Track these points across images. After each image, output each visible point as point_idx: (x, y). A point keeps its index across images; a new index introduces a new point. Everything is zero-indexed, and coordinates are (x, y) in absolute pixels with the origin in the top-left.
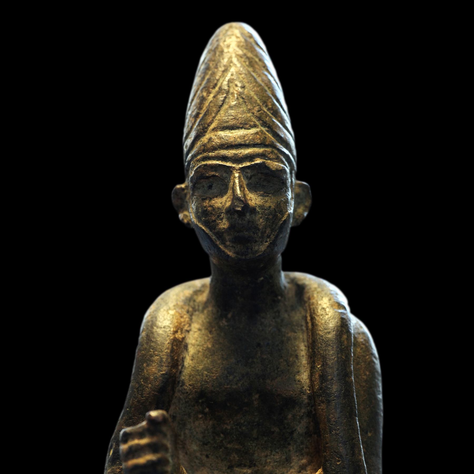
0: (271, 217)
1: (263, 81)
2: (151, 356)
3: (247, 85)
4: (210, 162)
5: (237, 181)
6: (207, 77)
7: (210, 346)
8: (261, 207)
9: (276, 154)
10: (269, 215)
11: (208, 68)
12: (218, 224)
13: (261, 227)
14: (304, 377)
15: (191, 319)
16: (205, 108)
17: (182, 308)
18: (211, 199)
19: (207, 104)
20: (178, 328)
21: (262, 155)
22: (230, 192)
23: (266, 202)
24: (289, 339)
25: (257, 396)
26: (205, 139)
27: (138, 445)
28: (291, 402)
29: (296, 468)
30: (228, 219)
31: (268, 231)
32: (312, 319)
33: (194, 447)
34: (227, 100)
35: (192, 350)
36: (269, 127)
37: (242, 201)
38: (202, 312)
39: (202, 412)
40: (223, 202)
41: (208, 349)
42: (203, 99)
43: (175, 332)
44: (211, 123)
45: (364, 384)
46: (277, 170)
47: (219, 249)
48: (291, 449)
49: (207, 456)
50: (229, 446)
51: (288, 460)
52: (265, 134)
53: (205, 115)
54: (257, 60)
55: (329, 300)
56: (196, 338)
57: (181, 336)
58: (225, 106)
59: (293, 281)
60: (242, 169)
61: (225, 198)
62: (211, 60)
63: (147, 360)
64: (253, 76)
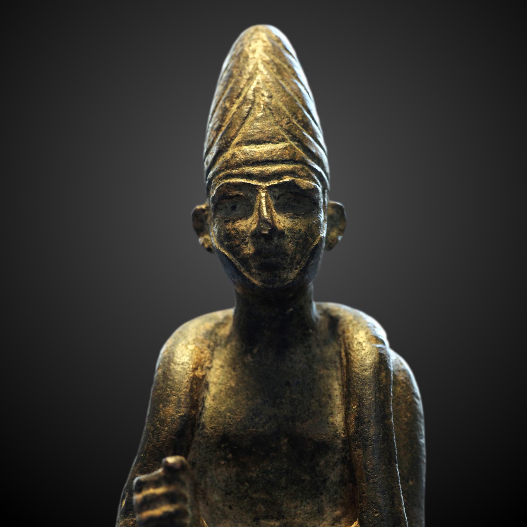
0: (301, 241)
1: (292, 90)
2: (168, 396)
3: (274, 94)
4: (233, 180)
5: (263, 201)
6: (230, 86)
7: (233, 385)
8: (290, 230)
9: (307, 171)
10: (299, 239)
11: (231, 76)
12: (242, 250)
13: (290, 253)
14: (338, 419)
15: (212, 355)
16: (227, 120)
17: (202, 342)
18: (234, 221)
19: (230, 115)
20: (198, 365)
21: (291, 173)
22: (255, 213)
23: (296, 224)
24: (321, 377)
25: (286, 441)
26: (227, 155)
27: (153, 495)
28: (323, 447)
29: (330, 520)
30: (253, 244)
31: (298, 257)
32: (347, 354)
33: (216, 497)
34: (252, 111)
35: (213, 390)
36: (299, 141)
37: (270, 224)
38: (225, 346)
39: (225, 458)
40: (247, 225)
41: (231, 388)
42: (225, 111)
43: (195, 369)
44: (235, 136)
45: (405, 427)
46: (308, 189)
47: (243, 277)
48: (324, 499)
49: (230, 507)
50: (254, 496)
51: (320, 512)
52: (295, 149)
53: (228, 128)
54: (286, 67)
55: (366, 334)
56: (217, 376)
57: (201, 374)
58: (251, 118)
59: (326, 313)
60: (269, 188)
61: (250, 220)
62: (234, 67)
63: (162, 399)
64: (281, 85)
